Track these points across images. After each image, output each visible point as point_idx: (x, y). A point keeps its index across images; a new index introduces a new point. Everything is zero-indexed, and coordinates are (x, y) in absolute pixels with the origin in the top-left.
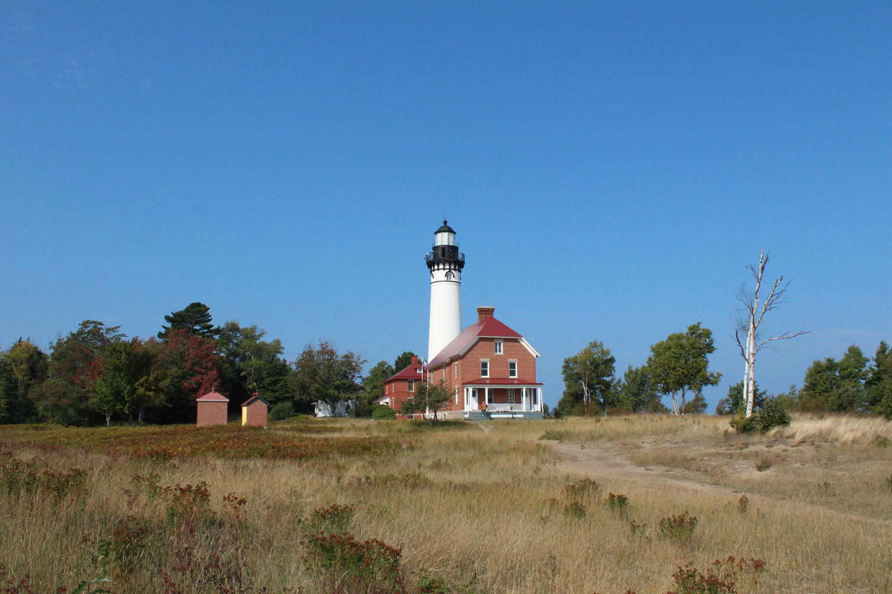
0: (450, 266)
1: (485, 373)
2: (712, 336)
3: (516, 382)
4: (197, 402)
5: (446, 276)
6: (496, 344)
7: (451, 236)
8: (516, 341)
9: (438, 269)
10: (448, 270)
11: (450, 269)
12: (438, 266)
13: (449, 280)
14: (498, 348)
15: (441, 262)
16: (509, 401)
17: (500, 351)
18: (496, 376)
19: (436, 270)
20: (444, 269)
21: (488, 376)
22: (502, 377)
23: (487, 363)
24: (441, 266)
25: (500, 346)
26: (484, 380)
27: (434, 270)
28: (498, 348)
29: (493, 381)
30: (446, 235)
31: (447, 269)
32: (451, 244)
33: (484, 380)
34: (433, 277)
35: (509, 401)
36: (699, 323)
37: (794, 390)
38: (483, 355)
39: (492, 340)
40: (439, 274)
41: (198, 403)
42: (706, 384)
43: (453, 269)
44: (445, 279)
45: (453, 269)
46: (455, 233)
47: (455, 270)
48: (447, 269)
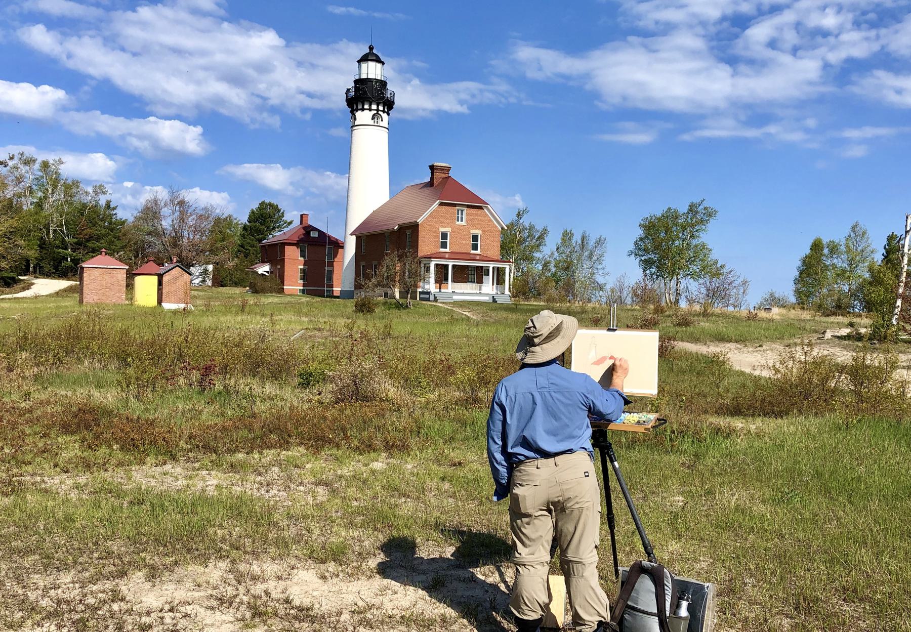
0: (378, 107)
1: (444, 245)
2: (825, 241)
3: (447, 256)
4: (82, 268)
5: (373, 119)
6: (458, 210)
7: (379, 65)
8: (480, 208)
9: (363, 109)
10: (376, 112)
11: (378, 110)
12: (370, 105)
13: (376, 124)
14: (460, 216)
15: (360, 101)
16: (470, 280)
17: (462, 221)
18: (457, 249)
19: (360, 109)
20: (370, 110)
21: (447, 250)
22: (463, 251)
23: (447, 234)
24: (374, 107)
25: (462, 214)
26: (443, 254)
27: (357, 110)
28: (460, 216)
29: (454, 255)
30: (372, 64)
31: (374, 110)
32: (379, 78)
33: (443, 254)
34: (382, 121)
35: (470, 280)
36: (893, 233)
37: (253, 224)
38: (443, 224)
39: (455, 205)
40: (364, 116)
41: (85, 269)
42: (357, 111)
43: (381, 111)
44: (372, 122)
45: (381, 111)
46: (383, 63)
47: (384, 111)
48: (374, 110)
